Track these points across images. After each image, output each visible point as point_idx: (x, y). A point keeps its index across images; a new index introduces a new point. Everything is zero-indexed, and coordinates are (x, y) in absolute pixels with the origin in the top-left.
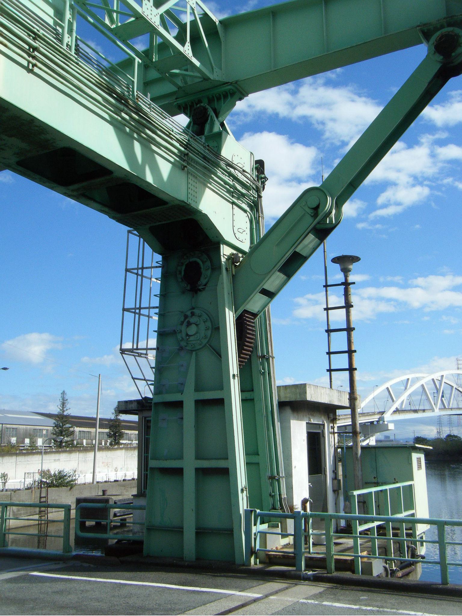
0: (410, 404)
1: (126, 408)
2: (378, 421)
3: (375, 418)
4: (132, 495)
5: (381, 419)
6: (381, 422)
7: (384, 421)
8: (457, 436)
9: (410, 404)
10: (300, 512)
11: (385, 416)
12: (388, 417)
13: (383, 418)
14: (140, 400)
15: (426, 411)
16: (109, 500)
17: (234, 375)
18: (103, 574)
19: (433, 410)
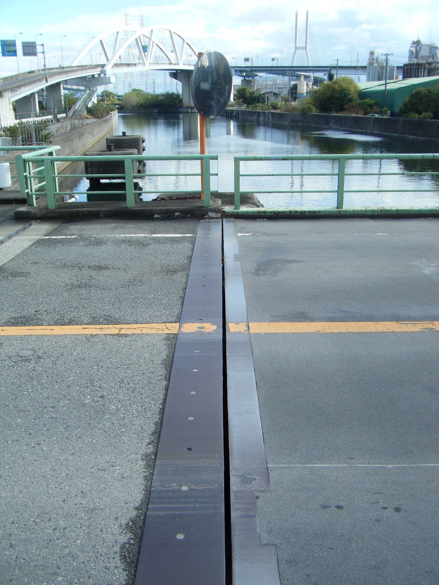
0: (120, 58)
1: (301, 194)
2: (99, 75)
3: (96, 72)
4: (176, 74)
5: (103, 72)
6: (102, 75)
7: (105, 75)
8: (141, 90)
9: (120, 58)
10: (304, 93)
11: (106, 70)
12: (109, 70)
13: (105, 71)
14: (84, 203)
15: (137, 65)
16: (139, 139)
17: (203, 328)
18: (309, 189)
19: (144, 64)
